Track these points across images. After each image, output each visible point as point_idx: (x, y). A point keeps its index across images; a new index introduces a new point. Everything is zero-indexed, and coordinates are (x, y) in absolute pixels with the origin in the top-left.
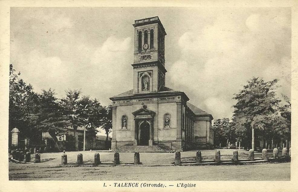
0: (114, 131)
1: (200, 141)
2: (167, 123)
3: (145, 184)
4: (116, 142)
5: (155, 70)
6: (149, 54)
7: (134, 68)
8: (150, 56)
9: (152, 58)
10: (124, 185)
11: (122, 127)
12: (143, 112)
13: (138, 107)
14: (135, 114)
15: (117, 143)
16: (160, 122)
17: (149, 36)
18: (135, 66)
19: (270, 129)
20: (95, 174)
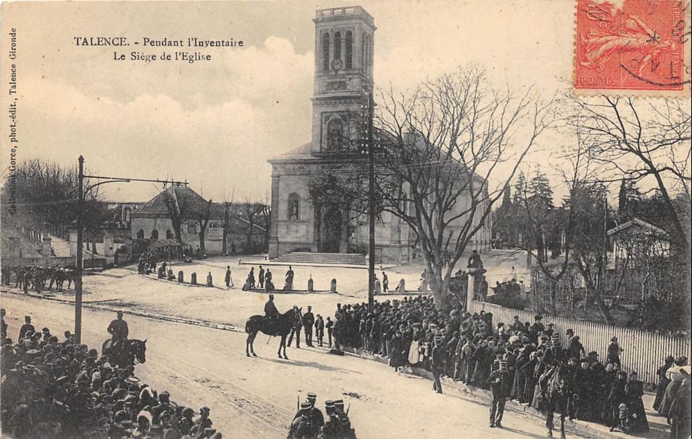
3: (11, 168)
4: (278, 243)
6: (344, 80)
9: (348, 87)
15: (280, 246)
17: (343, 45)
19: (152, 354)
20: (8, 294)
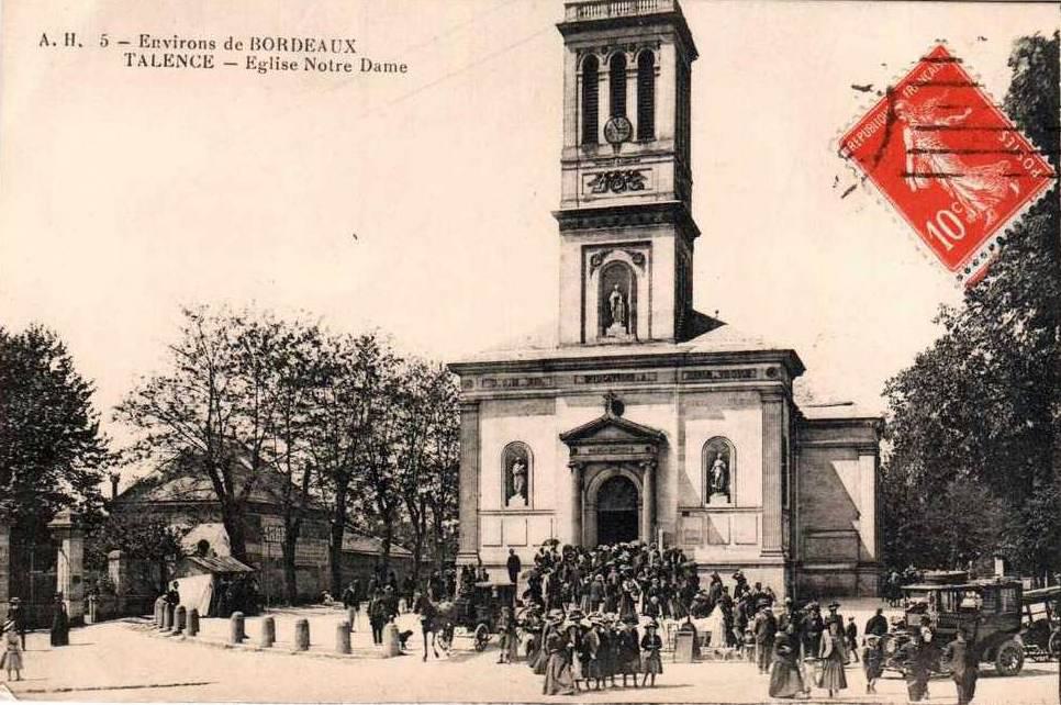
0: (676, 379)
1: (514, 564)
2: (719, 481)
5: (664, 244)
7: (562, 229)
8: (637, 173)
10: (160, 60)
11: (508, 497)
12: (611, 433)
13: (591, 413)
14: (573, 439)
16: (686, 469)
18: (572, 221)
